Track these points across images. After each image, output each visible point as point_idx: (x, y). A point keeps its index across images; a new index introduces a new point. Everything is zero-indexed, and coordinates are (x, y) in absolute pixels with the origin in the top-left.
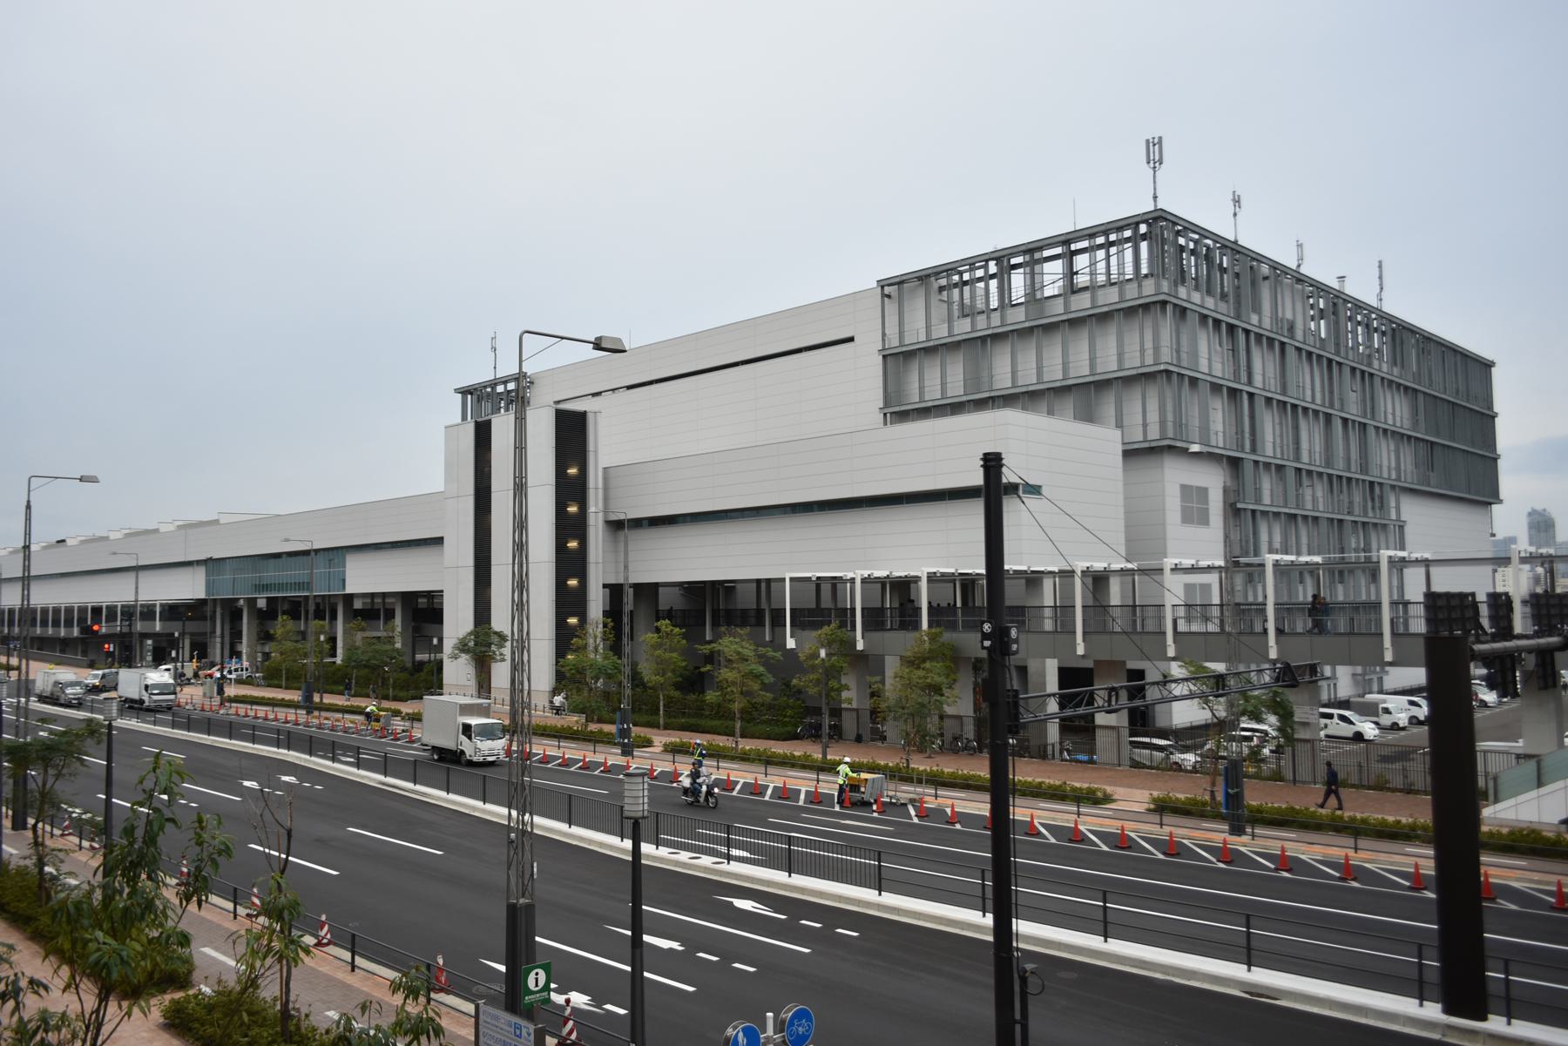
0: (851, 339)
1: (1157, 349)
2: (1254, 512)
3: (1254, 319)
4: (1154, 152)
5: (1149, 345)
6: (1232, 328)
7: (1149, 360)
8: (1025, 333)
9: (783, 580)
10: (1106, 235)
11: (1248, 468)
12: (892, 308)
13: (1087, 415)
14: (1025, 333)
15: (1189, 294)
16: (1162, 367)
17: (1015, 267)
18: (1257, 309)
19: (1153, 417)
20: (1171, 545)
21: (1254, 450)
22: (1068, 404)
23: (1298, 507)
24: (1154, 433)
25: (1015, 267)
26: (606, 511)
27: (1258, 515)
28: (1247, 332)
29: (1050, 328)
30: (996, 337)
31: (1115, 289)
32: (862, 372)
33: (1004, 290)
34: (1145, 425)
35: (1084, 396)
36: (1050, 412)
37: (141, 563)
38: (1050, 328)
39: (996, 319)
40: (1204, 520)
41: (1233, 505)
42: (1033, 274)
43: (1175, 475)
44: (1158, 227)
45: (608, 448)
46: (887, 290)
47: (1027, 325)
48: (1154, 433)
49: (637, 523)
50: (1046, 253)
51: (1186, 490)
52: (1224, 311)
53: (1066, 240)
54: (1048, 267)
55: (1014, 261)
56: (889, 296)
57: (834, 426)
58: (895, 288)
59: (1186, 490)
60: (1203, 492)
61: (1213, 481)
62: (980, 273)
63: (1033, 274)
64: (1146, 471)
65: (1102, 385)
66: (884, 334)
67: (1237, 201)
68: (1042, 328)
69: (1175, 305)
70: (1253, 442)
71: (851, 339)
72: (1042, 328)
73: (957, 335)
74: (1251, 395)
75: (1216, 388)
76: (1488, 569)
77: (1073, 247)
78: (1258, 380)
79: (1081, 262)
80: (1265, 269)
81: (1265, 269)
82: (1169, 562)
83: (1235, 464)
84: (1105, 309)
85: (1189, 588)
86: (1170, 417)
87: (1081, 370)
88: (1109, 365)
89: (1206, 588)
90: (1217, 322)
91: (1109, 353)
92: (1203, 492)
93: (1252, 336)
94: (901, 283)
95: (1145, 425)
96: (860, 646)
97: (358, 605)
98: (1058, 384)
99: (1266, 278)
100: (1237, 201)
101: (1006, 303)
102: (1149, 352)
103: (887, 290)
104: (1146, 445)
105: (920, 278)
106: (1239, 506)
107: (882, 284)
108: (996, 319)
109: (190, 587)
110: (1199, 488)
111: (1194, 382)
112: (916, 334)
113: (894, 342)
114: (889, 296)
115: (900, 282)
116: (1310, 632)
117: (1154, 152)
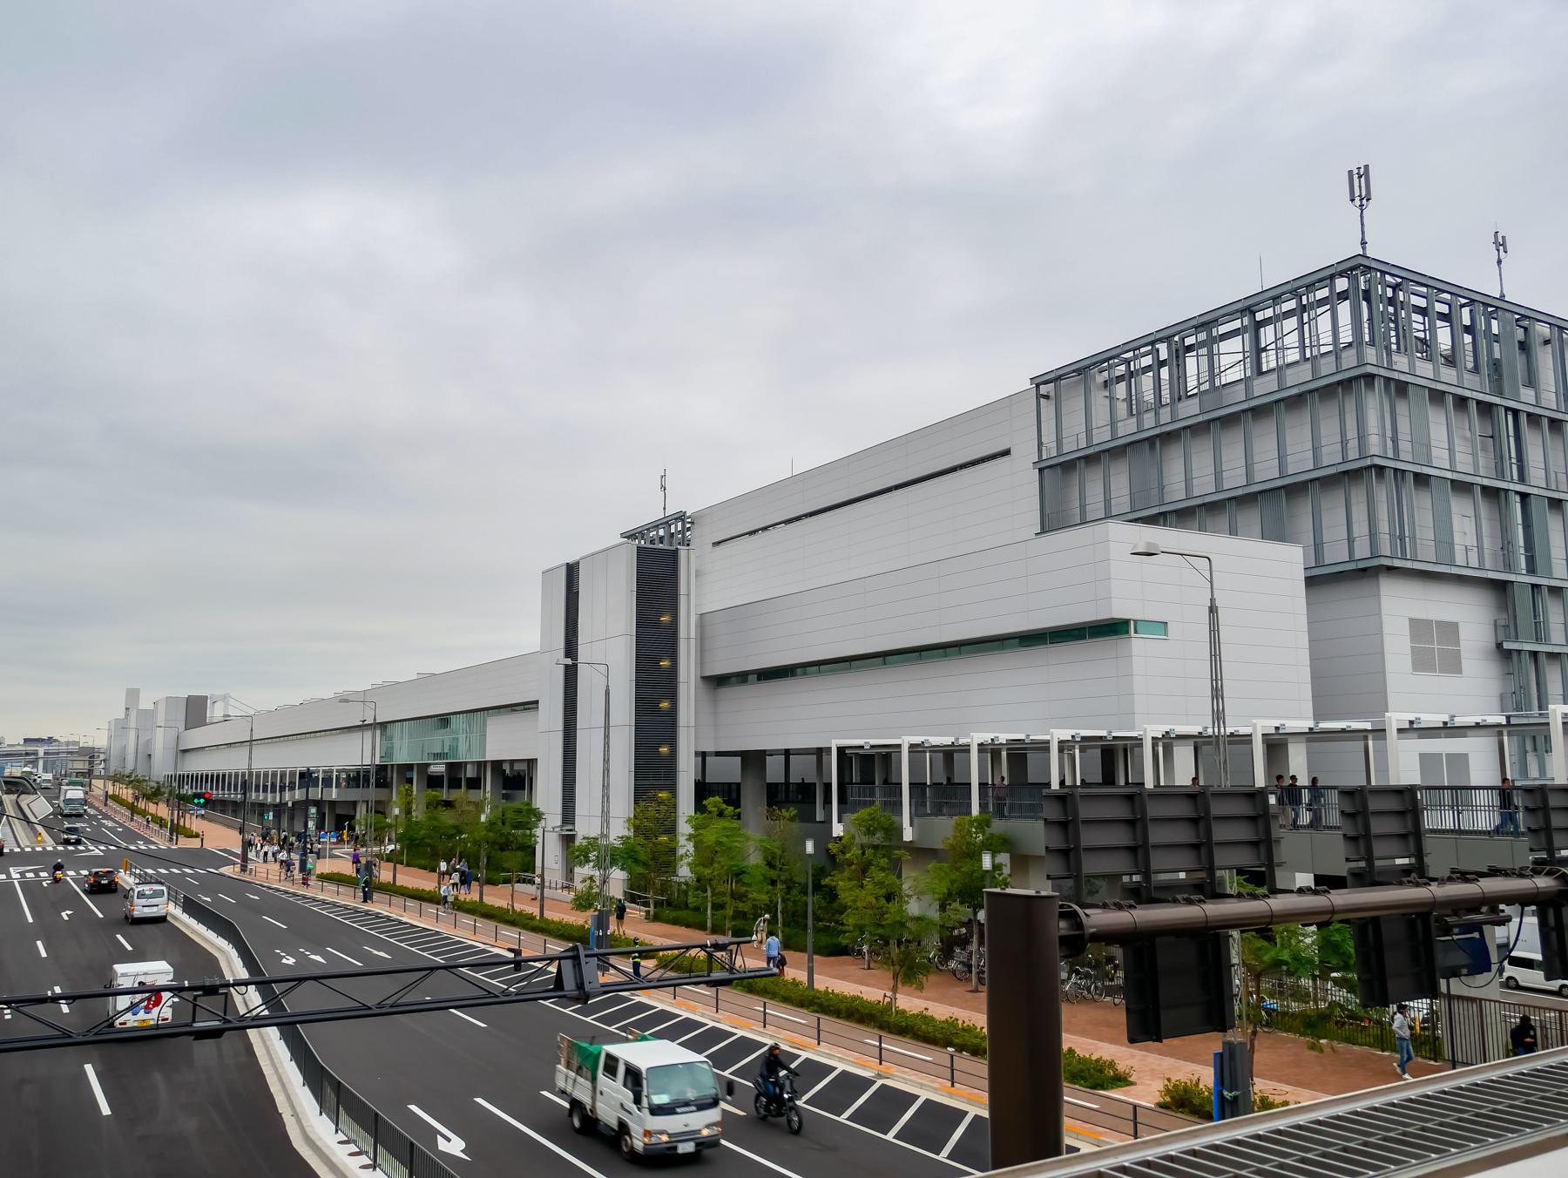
0: (1007, 453)
1: (1362, 438)
2: (1535, 654)
3: (1527, 395)
4: (1360, 186)
5: (1352, 434)
6: (1486, 409)
7: (1353, 453)
8: (1199, 429)
9: (830, 749)
10: (1302, 294)
11: (1523, 599)
12: (1048, 409)
13: (1276, 532)
14: (1199, 429)
15: (1412, 365)
16: (1368, 462)
17: (1190, 348)
18: (1531, 381)
19: (1361, 528)
20: (1392, 699)
21: (1531, 570)
22: (1251, 517)
23: (1538, 640)
24: (1362, 550)
25: (1190, 348)
26: (701, 662)
27: (1542, 658)
28: (1516, 412)
29: (1229, 421)
30: (1168, 438)
31: (1308, 365)
32: (1017, 485)
33: (1180, 376)
34: (1351, 541)
35: (1270, 505)
36: (1233, 532)
37: (560, 725)
38: (1229, 421)
39: (1165, 415)
40: (1452, 665)
41: (1499, 646)
42: (1211, 356)
43: (1399, 607)
44: (1362, 279)
45: (707, 588)
46: (1044, 389)
47: (1201, 419)
48: (1362, 550)
49: (742, 677)
50: (1223, 329)
51: (1419, 628)
52: (1475, 387)
53: (1247, 308)
54: (1224, 346)
55: (1189, 341)
56: (1047, 397)
57: (993, 557)
58: (1051, 386)
59: (1419, 628)
60: (1450, 630)
61: (1471, 617)
62: (1147, 361)
63: (1211, 356)
64: (1345, 603)
65: (1295, 490)
66: (1040, 444)
67: (1500, 244)
68: (1226, 420)
69: (1387, 380)
70: (1531, 560)
71: (1007, 453)
72: (1226, 420)
73: (1135, 436)
74: (1524, 497)
75: (1462, 487)
76: (245, 751)
77: (1259, 316)
78: (1536, 475)
79: (1267, 335)
80: (1543, 330)
81: (1543, 330)
82: (1396, 718)
83: (1501, 589)
84: (1295, 391)
85: (1426, 760)
86: (1384, 527)
87: (1267, 472)
88: (1301, 463)
89: (1459, 761)
90: (1461, 402)
91: (1301, 447)
92: (1450, 630)
93: (1523, 419)
94: (1059, 378)
95: (1351, 541)
96: (908, 835)
97: (774, 771)
98: (1240, 492)
99: (1547, 342)
100: (1500, 244)
101: (1181, 395)
102: (1353, 445)
103: (1044, 389)
104: (1352, 566)
105: (1079, 371)
106: (1506, 646)
107: (1038, 382)
108: (1165, 415)
109: (356, 753)
110: (1442, 625)
111: (1422, 480)
112: (1075, 442)
113: (1050, 450)
114: (1047, 397)
115: (1056, 378)
116: (1497, 831)
117: (1360, 186)
